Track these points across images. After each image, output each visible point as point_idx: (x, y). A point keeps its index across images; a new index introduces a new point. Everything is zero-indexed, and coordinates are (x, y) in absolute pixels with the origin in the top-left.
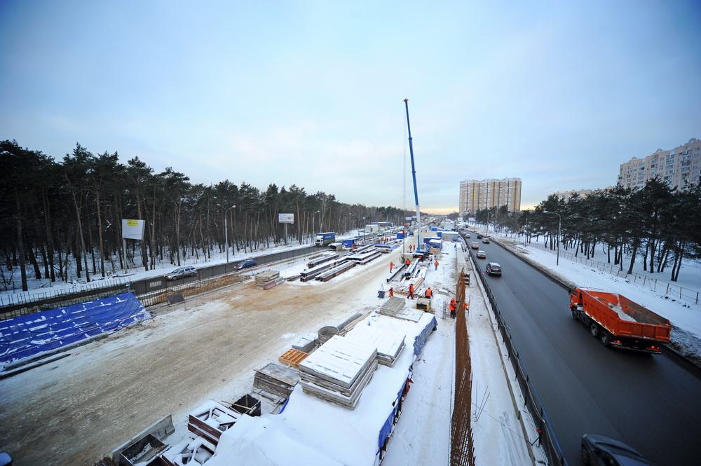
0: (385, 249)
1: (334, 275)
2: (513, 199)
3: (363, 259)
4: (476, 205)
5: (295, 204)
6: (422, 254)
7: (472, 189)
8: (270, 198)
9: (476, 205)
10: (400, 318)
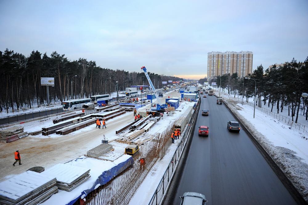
0: (130, 107)
1: (74, 130)
2: (247, 68)
3: (106, 116)
4: (220, 72)
5: (57, 69)
6: (155, 111)
7: (217, 59)
8: (31, 63)
9: (220, 72)
10: (101, 159)
